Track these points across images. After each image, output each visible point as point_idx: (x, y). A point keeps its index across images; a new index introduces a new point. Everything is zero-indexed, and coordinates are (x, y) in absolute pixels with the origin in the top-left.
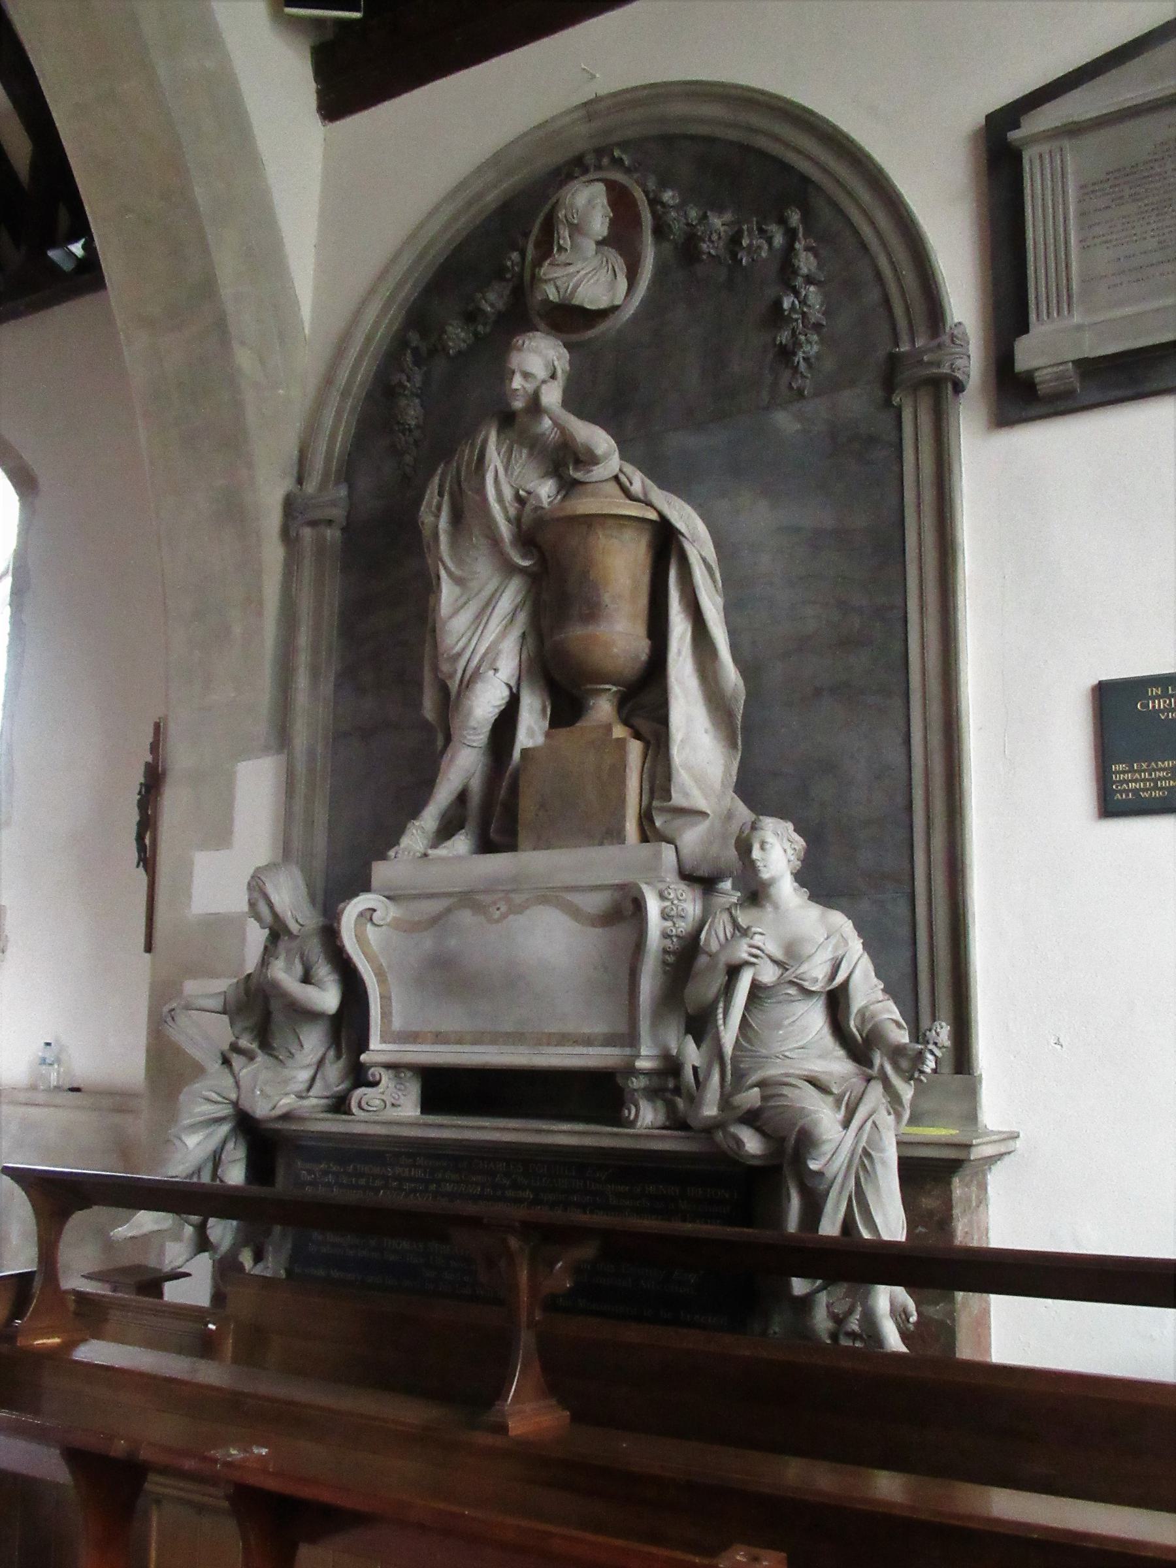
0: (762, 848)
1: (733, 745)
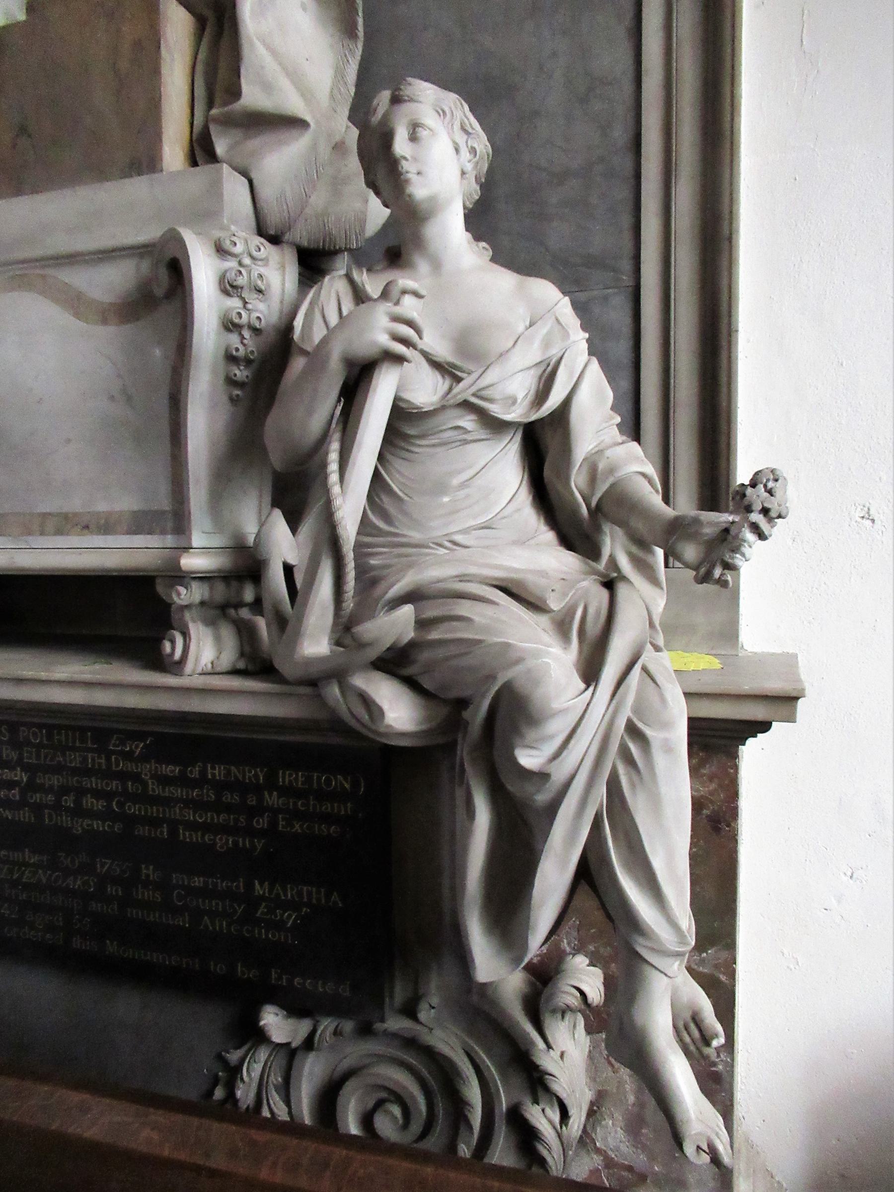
0: (413, 138)
1: (349, 31)
